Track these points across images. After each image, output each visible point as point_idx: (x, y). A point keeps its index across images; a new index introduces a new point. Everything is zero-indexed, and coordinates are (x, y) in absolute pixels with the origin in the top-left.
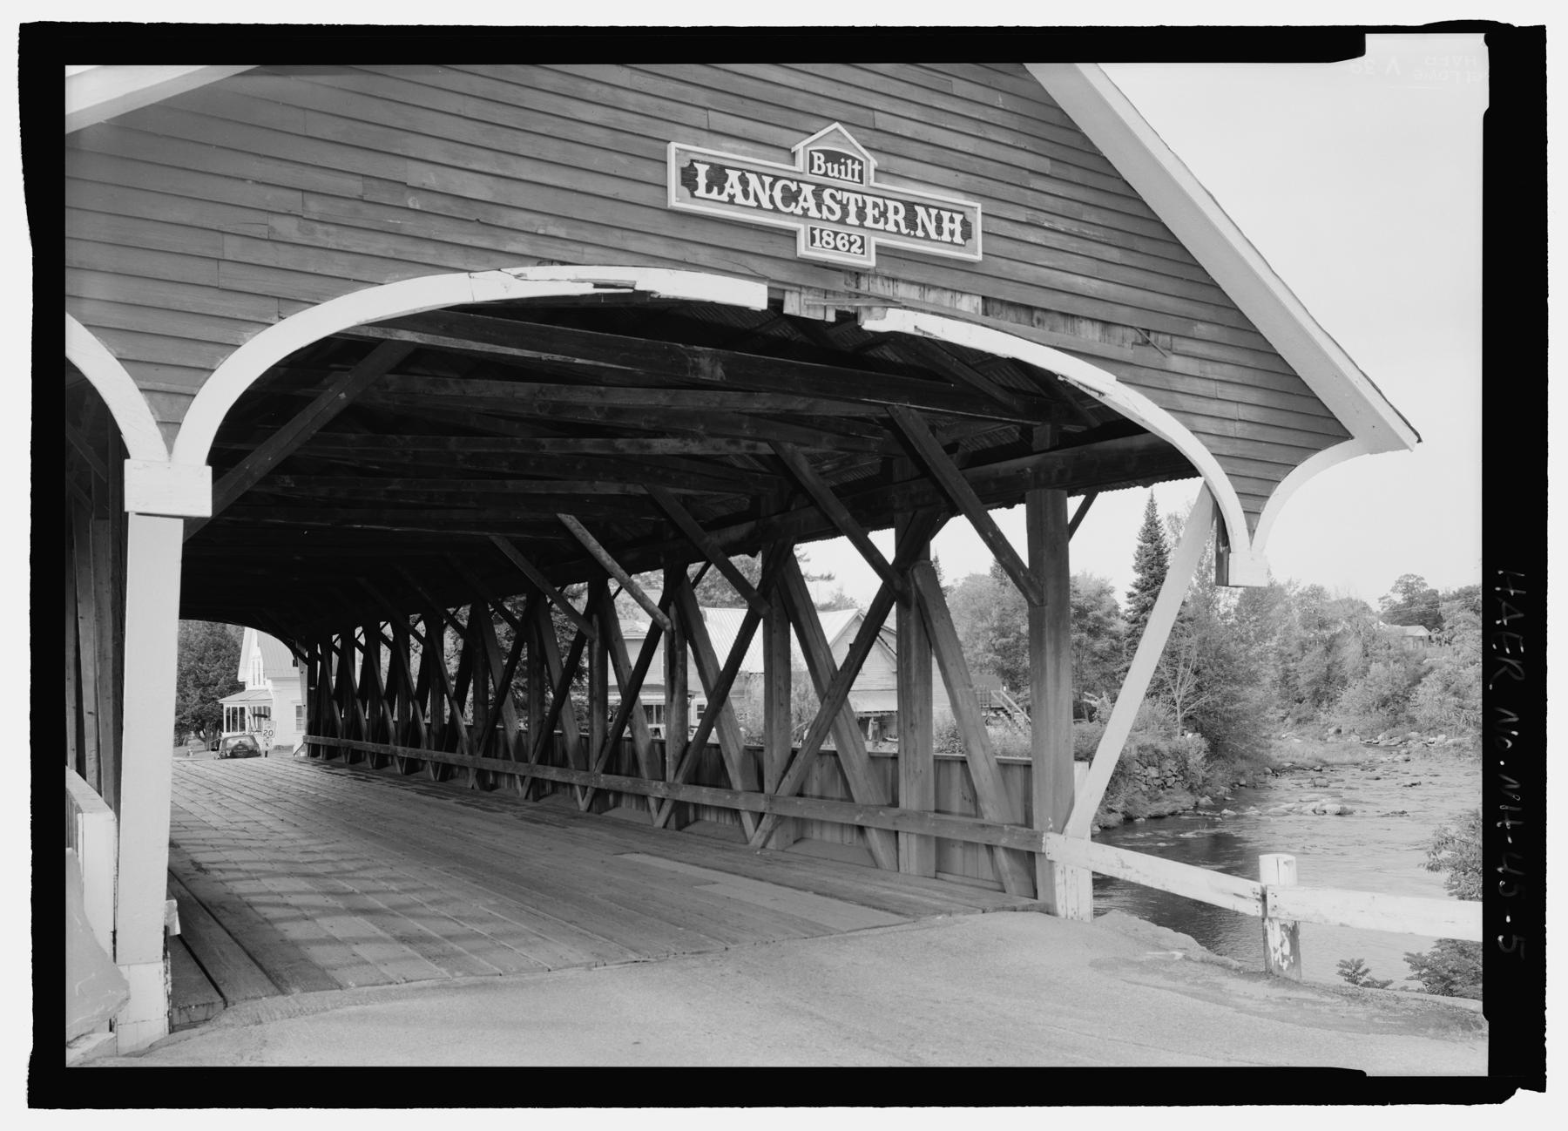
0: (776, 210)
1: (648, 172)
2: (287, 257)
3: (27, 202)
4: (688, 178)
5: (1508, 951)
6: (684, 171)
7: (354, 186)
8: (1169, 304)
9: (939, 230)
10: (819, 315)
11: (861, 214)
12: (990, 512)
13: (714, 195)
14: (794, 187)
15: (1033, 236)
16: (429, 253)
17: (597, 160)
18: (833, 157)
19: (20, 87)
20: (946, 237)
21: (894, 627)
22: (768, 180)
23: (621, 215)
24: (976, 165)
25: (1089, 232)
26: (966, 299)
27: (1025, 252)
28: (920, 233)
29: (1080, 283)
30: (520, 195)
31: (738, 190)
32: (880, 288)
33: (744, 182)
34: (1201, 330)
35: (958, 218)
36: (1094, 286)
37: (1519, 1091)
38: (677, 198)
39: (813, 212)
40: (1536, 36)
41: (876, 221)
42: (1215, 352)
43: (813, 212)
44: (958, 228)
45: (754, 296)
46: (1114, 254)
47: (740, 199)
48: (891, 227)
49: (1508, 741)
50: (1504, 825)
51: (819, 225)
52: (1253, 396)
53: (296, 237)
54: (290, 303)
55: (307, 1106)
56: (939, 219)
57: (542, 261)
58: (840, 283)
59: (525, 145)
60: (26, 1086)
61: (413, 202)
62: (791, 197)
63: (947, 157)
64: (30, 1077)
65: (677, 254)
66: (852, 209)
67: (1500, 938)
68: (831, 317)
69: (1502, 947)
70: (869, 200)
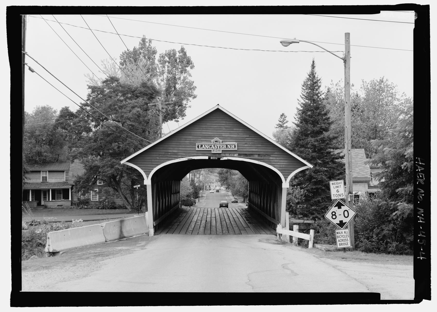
0: (209, 148)
1: (194, 146)
2: (157, 161)
4: (198, 147)
6: (198, 146)
7: (164, 153)
8: (270, 150)
9: (231, 147)
10: (215, 159)
11: (220, 147)
13: (201, 148)
14: (211, 145)
15: (246, 145)
16: (171, 158)
17: (188, 146)
18: (216, 141)
19: (7, 37)
20: (232, 148)
22: (208, 145)
23: (191, 152)
24: (237, 138)
25: (255, 143)
26: (236, 154)
27: (245, 147)
28: (228, 148)
29: (254, 150)
30: (180, 151)
31: (204, 147)
32: (223, 155)
33: (205, 146)
34: (276, 153)
35: (234, 145)
36: (256, 150)
37: (424, 300)
38: (197, 149)
39: (213, 148)
40: (427, 7)
41: (222, 147)
42: (279, 156)
43: (213, 148)
44: (234, 146)
45: (207, 158)
46: (260, 145)
47: (204, 148)
48: (224, 148)
50: (418, 171)
51: (214, 149)
52: (286, 161)
53: (159, 159)
54: (158, 165)
56: (231, 146)
57: (182, 158)
58: (217, 155)
59: (180, 146)
61: (169, 154)
62: (210, 147)
63: (234, 138)
65: (197, 155)
66: (219, 147)
68: (217, 159)
70: (221, 145)
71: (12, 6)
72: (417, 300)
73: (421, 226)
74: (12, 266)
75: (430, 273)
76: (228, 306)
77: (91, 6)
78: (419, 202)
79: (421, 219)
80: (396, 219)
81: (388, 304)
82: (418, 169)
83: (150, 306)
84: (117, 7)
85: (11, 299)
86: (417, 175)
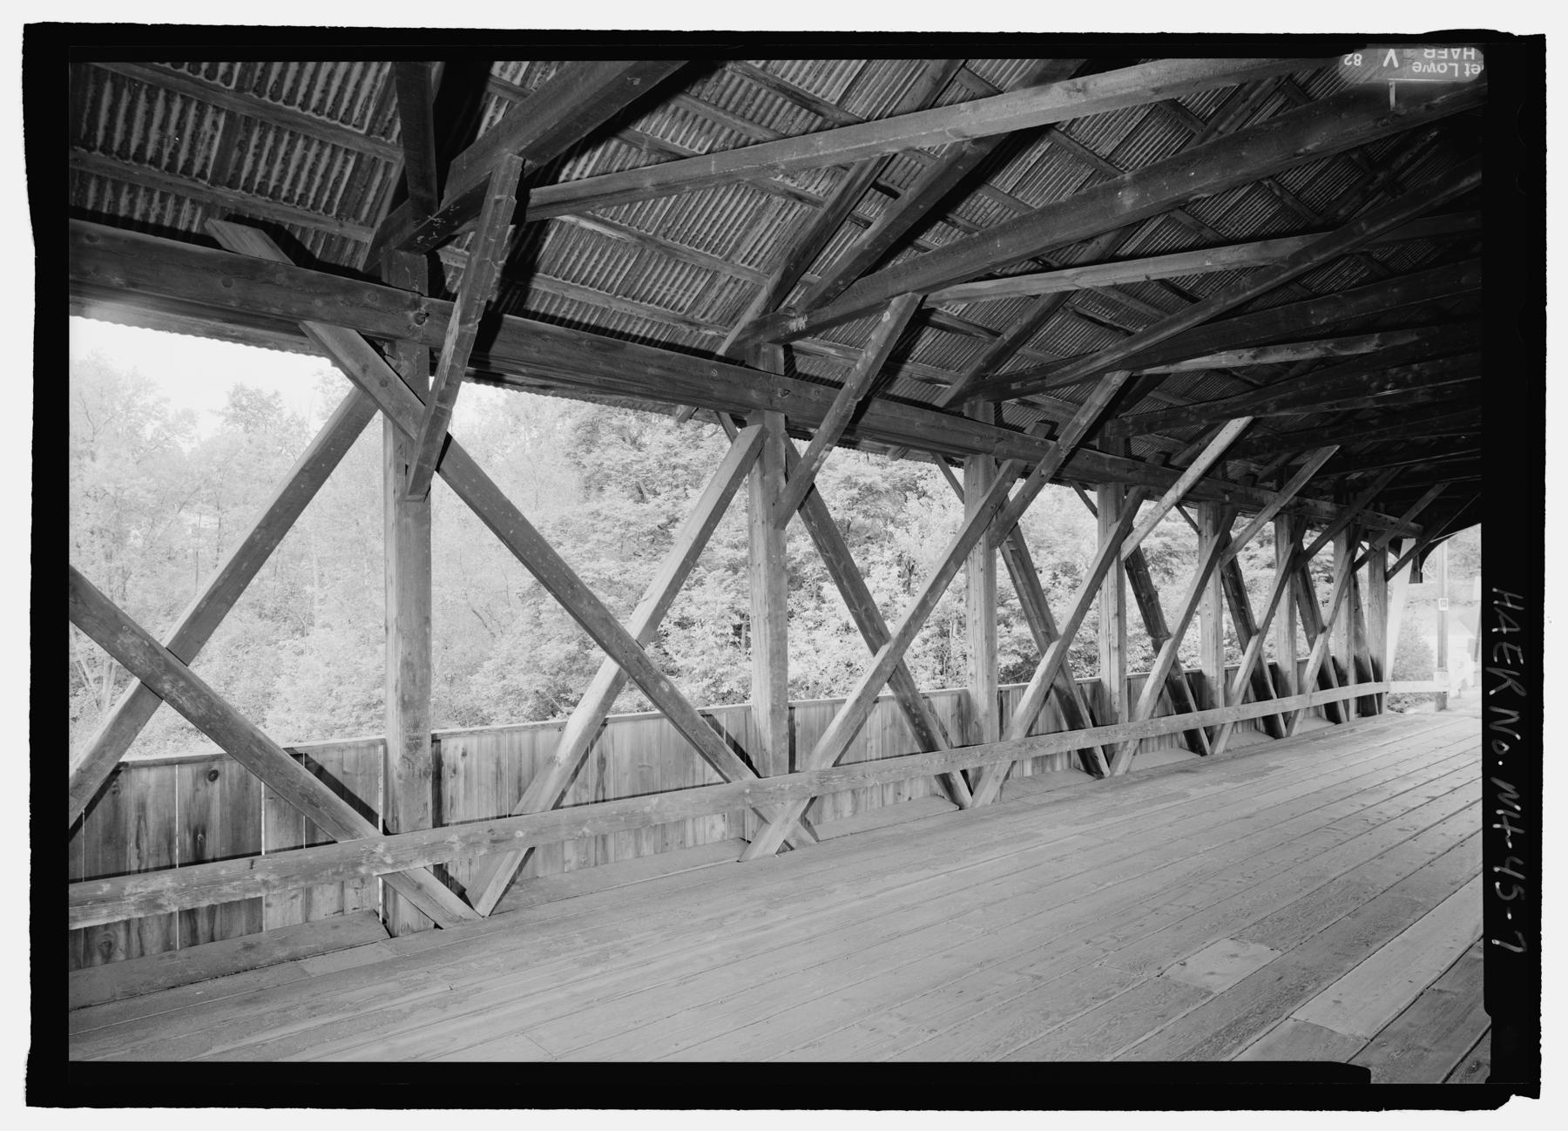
3: (30, 203)
12: (1479, 526)
19: (23, 87)
21: (1360, 549)
37: (1514, 1096)
49: (1504, 745)
55: (304, 1106)
60: (24, 1084)
64: (28, 1075)
69: (1500, 894)
72: (1487, 1097)
73: (1508, 909)
76: (808, 1112)
77: (327, 25)
78: (1500, 763)
79: (1509, 597)
80: (357, 872)
81: (1384, 1112)
83: (240, 1106)
84: (805, 32)
85: (1545, 150)
86: (1495, 652)
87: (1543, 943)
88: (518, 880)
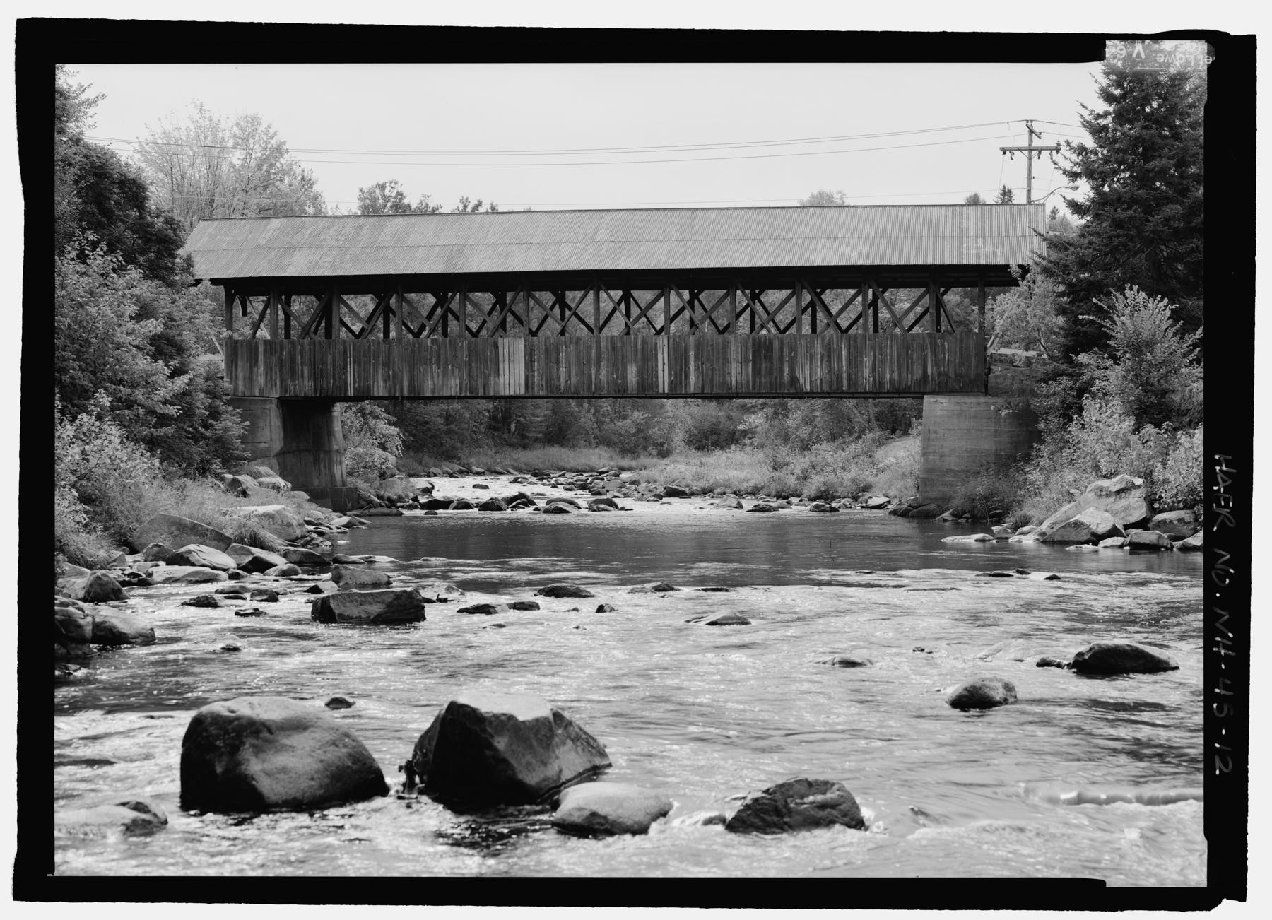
5: (1223, 715)
37: (1225, 901)
40: (1249, 43)
60: (11, 882)
67: (1215, 706)
71: (33, 19)
74: (944, 34)
75: (1246, 821)
77: (263, 21)
78: (1218, 595)
81: (1119, 912)
82: (1217, 484)
84: (341, 25)
85: (15, 879)
87: (1250, 775)
88: (953, 298)
